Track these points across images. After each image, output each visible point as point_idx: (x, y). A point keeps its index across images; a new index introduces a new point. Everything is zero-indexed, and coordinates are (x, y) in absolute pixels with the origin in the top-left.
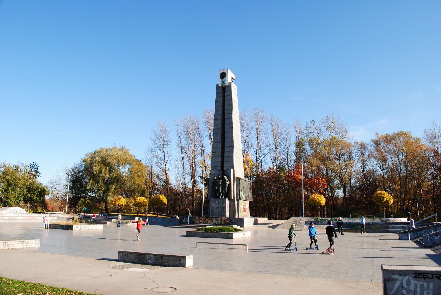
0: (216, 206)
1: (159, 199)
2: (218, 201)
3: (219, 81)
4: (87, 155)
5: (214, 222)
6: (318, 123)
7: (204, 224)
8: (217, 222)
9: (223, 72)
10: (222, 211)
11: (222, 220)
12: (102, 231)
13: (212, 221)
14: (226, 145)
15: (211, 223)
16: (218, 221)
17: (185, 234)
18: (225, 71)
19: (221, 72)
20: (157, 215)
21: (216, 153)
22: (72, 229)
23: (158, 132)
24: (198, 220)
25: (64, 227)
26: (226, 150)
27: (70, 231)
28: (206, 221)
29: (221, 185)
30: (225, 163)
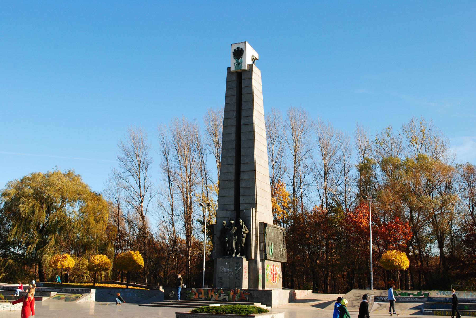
0: (225, 270)
2: (228, 263)
3: (231, 63)
5: (222, 297)
7: (206, 300)
8: (227, 297)
14: (243, 168)
15: (217, 299)
16: (229, 295)
18: (241, 46)
19: (235, 47)
20: (127, 285)
21: (227, 182)
24: (195, 294)
26: (243, 177)
28: (210, 296)
29: (235, 235)
30: (241, 198)
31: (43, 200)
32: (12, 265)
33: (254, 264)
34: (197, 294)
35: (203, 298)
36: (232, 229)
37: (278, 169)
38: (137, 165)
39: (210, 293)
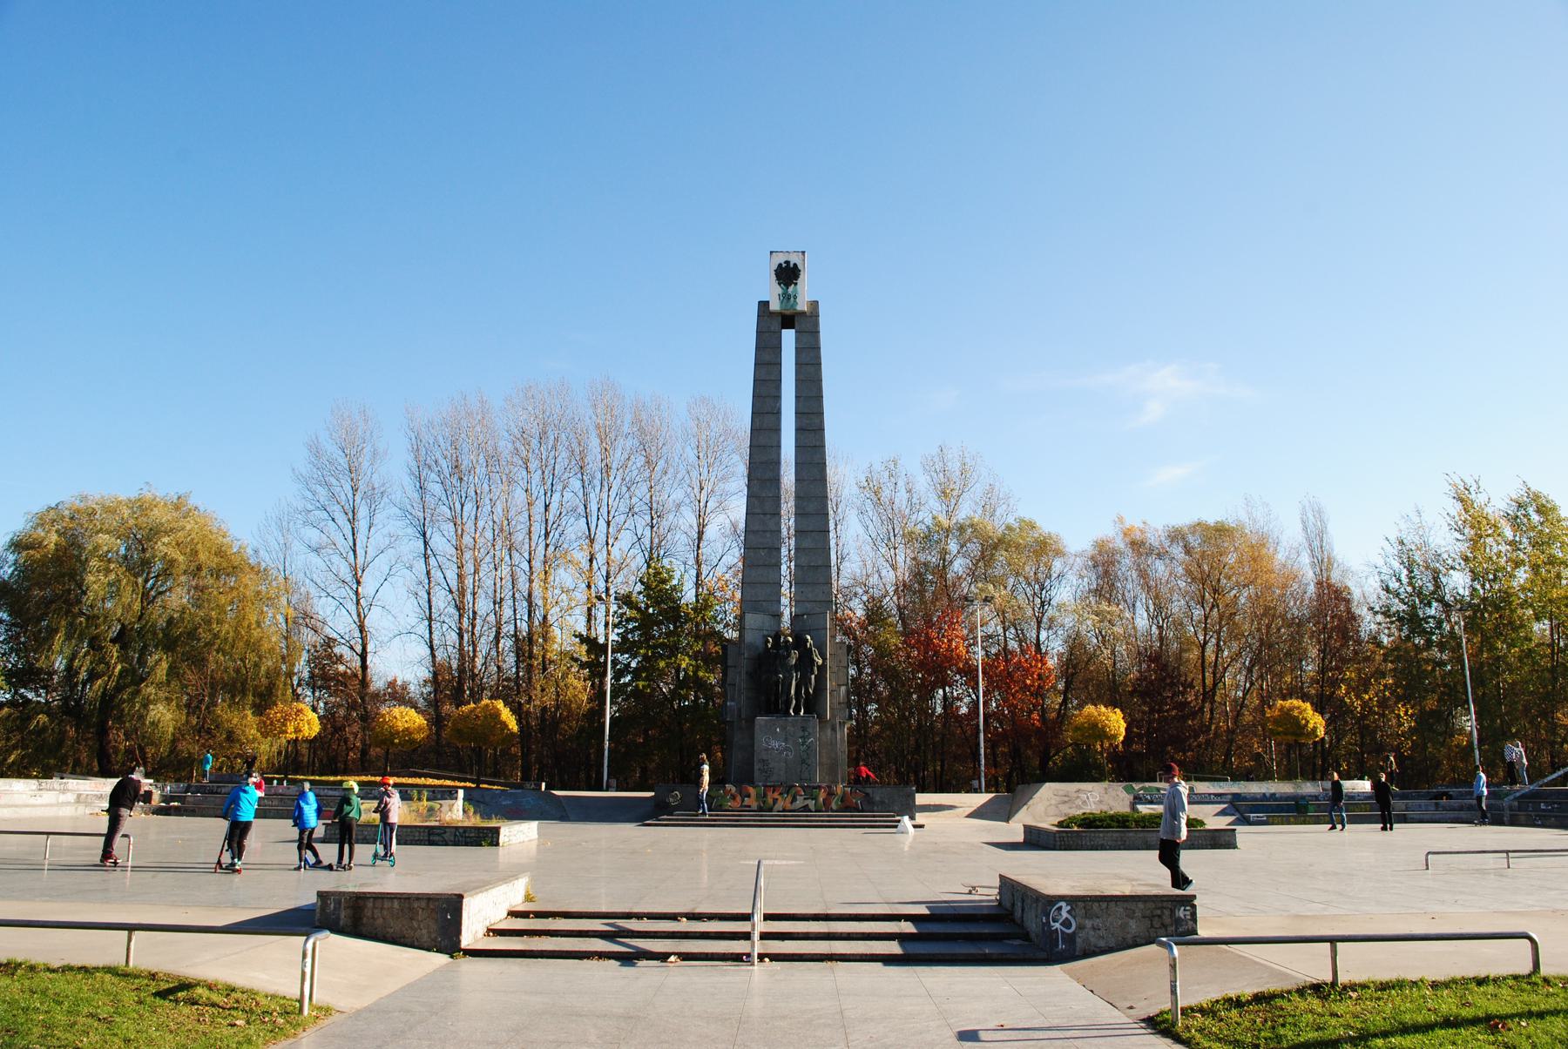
0: (775, 744)
1: (497, 714)
2: (783, 729)
3: (771, 292)
4: (41, 521)
5: (800, 803)
6: (877, 467)
7: (760, 809)
8: (811, 803)
9: (787, 262)
10: (803, 762)
11: (831, 794)
12: (534, 846)
13: (794, 800)
15: (789, 806)
16: (815, 799)
17: (1020, 838)
18: (794, 259)
19: (781, 259)
20: (478, 782)
22: (495, 843)
23: (331, 449)
24: (733, 797)
25: (446, 836)
27: (483, 852)
28: (770, 801)
29: (797, 667)
31: (140, 557)
32: (45, 728)
33: (829, 732)
34: (739, 798)
35: (755, 806)
36: (789, 655)
37: (520, 537)
38: (344, 491)
39: (770, 794)
